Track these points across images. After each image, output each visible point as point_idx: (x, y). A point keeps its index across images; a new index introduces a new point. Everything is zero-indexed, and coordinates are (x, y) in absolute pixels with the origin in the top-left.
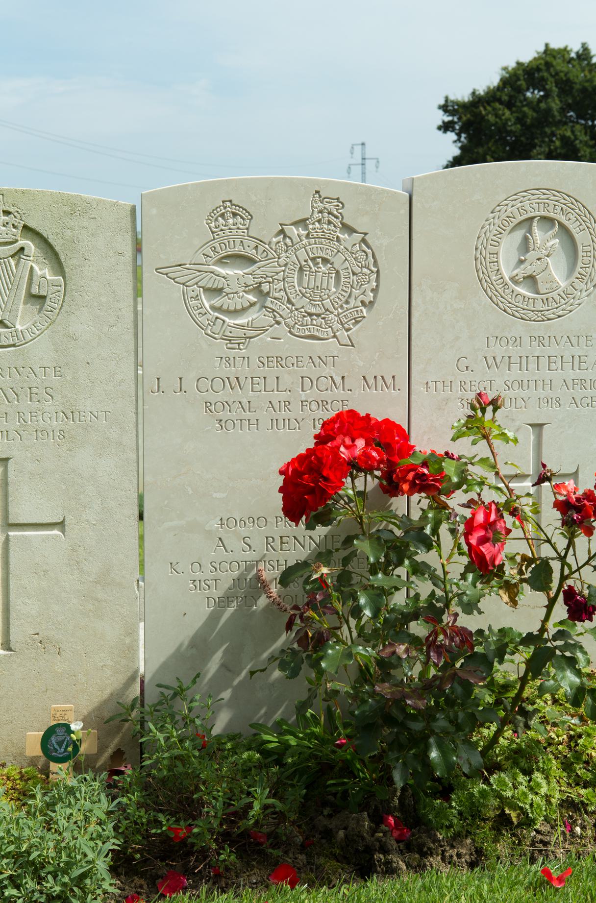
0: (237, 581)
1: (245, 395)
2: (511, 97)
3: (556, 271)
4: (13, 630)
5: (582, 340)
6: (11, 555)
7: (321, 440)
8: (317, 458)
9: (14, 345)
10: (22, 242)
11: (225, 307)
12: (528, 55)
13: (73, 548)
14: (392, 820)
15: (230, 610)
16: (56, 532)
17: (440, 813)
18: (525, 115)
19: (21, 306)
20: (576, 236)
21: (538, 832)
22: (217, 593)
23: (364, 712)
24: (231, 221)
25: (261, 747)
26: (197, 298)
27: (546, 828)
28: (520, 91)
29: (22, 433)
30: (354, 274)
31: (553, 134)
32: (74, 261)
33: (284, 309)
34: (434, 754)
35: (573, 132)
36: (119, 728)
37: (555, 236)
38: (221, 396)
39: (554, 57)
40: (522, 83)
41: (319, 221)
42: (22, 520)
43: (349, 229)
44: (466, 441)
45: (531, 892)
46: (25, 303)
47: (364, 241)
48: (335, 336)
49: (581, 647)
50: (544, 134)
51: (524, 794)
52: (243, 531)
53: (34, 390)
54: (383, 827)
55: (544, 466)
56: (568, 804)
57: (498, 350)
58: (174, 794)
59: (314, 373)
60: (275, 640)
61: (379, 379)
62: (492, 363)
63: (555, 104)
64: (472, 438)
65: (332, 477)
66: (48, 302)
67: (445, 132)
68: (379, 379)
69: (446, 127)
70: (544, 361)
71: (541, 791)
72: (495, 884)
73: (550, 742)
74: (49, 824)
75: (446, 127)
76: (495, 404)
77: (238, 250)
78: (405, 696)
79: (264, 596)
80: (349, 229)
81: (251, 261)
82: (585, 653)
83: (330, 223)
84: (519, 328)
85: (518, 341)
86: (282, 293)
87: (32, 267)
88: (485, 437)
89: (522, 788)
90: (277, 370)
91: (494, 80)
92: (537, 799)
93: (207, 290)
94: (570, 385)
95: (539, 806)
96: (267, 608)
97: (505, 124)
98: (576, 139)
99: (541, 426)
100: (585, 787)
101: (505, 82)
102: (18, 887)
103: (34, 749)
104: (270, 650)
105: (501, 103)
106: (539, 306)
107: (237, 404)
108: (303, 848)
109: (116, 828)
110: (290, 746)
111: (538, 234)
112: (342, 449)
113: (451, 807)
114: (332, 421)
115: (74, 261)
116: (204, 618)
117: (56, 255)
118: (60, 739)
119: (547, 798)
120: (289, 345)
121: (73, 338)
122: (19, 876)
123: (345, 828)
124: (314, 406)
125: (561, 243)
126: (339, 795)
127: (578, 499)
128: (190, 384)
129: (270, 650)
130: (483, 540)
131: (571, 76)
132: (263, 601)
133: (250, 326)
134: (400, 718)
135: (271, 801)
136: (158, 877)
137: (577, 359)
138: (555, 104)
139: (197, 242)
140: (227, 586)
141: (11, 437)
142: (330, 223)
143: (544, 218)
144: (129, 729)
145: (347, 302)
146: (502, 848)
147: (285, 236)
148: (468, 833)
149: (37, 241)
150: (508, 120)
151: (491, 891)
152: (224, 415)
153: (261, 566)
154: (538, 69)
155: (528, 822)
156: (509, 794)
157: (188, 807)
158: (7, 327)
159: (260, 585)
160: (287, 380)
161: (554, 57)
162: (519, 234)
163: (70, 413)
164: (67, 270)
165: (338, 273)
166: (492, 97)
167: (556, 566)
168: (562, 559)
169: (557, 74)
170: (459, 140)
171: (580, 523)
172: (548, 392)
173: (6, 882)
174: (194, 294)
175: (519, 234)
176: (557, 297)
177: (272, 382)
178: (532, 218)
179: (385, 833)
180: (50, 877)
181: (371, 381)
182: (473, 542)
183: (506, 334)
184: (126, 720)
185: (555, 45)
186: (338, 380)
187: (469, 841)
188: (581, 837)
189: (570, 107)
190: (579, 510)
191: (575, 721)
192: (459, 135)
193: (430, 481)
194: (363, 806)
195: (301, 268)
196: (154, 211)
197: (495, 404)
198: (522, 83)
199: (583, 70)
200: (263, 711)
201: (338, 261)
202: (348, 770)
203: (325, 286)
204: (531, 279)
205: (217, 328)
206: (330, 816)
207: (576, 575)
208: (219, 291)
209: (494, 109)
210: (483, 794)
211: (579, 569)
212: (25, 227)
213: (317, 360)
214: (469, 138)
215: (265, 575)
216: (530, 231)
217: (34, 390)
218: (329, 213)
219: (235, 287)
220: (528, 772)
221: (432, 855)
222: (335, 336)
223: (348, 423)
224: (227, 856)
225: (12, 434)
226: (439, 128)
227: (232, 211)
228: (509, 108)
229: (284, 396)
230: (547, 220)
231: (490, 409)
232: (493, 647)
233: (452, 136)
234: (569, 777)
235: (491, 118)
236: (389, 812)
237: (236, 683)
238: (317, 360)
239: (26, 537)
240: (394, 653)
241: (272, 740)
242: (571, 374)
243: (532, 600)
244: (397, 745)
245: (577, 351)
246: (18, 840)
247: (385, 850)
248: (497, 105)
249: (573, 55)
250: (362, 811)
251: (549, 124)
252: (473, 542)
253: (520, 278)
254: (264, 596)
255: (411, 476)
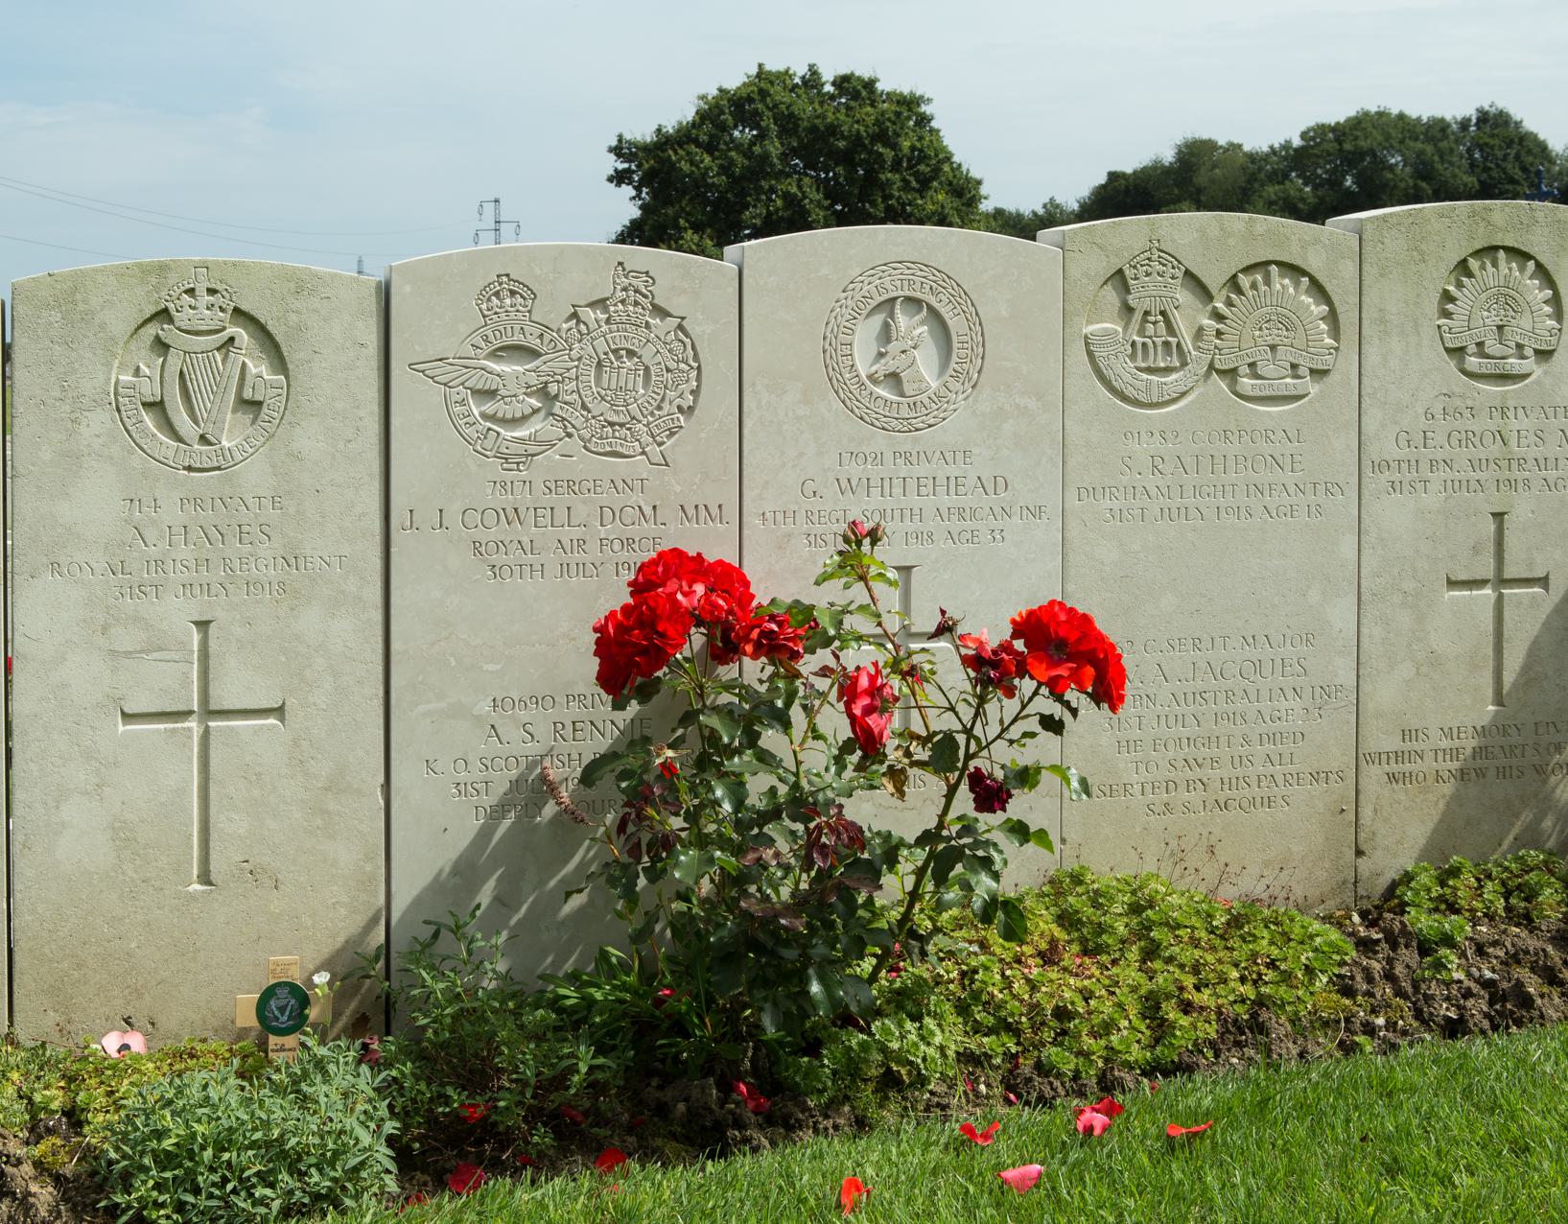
0: (516, 785)
1: (527, 532)
2: (711, 136)
3: (925, 365)
4: (214, 856)
5: (960, 456)
6: (212, 754)
7: (637, 588)
8: (649, 607)
9: (219, 468)
10: (231, 330)
11: (500, 415)
12: (735, 78)
13: (296, 742)
14: (743, 1088)
15: (507, 823)
16: (272, 721)
17: (810, 1073)
18: (732, 162)
19: (229, 416)
20: (950, 322)
21: (932, 1093)
22: (489, 801)
23: (721, 938)
24: (508, 301)
25: (555, 1004)
26: (463, 402)
27: (942, 1089)
28: (723, 128)
29: (228, 586)
30: (668, 370)
31: (772, 190)
32: (301, 355)
33: (577, 417)
34: (815, 988)
35: (800, 187)
36: (357, 988)
37: (922, 323)
38: (494, 533)
39: (772, 83)
40: (727, 117)
41: (623, 302)
42: (227, 705)
43: (661, 312)
44: (838, 583)
45: (953, 1154)
46: (234, 411)
47: (680, 327)
48: (644, 453)
49: (995, 845)
50: (759, 190)
51: (915, 1044)
52: (523, 715)
53: (246, 529)
54: (734, 1096)
55: (943, 612)
56: (967, 1057)
57: (855, 470)
58: (459, 1057)
59: (617, 500)
60: (566, 862)
61: (702, 508)
62: (846, 487)
63: (774, 148)
64: (844, 580)
65: (671, 632)
66: (265, 410)
67: (619, 185)
68: (702, 508)
69: (619, 178)
70: (912, 484)
71: (935, 1041)
72: (904, 1145)
73: (938, 981)
74: (304, 1101)
75: (619, 178)
76: (874, 536)
77: (518, 339)
78: (776, 916)
79: (552, 802)
80: (661, 312)
81: (534, 354)
82: (1001, 852)
83: (636, 303)
84: (880, 442)
85: (878, 458)
86: (575, 396)
87: (244, 364)
88: (863, 578)
89: (913, 1037)
90: (569, 498)
91: (689, 115)
92: (931, 1051)
93: (476, 392)
94: (945, 515)
95: (933, 1059)
96: (555, 820)
97: (705, 175)
98: (805, 197)
99: (909, 569)
100: (986, 1035)
101: (703, 116)
102: (272, 1186)
103: (248, 1019)
104: (559, 877)
105: (698, 145)
106: (905, 412)
107: (515, 544)
108: (630, 1130)
109: (391, 1107)
110: (596, 1001)
111: (902, 319)
112: (679, 596)
113: (823, 1066)
114: (653, 563)
115: (301, 355)
116: (471, 835)
117: (276, 347)
118: (283, 1002)
119: (942, 1049)
120: (584, 465)
121: (298, 457)
122: (271, 1171)
123: (686, 1100)
124: (617, 546)
125: (930, 332)
126: (669, 1061)
127: (994, 652)
128: (453, 518)
129: (559, 877)
130: (869, 710)
131: (794, 108)
132: (550, 810)
133: (533, 439)
134: (770, 944)
135: (601, 1061)
136: (446, 1171)
137: (953, 481)
138: (774, 148)
139: (464, 329)
140: (502, 790)
141: (213, 592)
142: (636, 303)
143: (908, 299)
144: (370, 989)
145: (659, 408)
146: (889, 1116)
147: (579, 321)
148: (847, 1098)
149: (251, 329)
150: (707, 169)
151: (902, 1154)
152: (498, 559)
153: (547, 763)
154: (750, 99)
155: (921, 1081)
156: (895, 1045)
157: (477, 1076)
158: (210, 444)
159: (546, 787)
160: (581, 512)
161: (772, 83)
162: (878, 319)
163: (292, 559)
164: (290, 367)
165: (647, 369)
166: (684, 137)
167: (961, 739)
168: (968, 732)
169: (776, 106)
170: (638, 196)
171: (997, 683)
172: (916, 525)
173: (254, 1180)
174: (459, 398)
175: (878, 319)
176: (926, 401)
177: (561, 515)
178: (895, 299)
179: (737, 1104)
180: (313, 1170)
181: (691, 512)
182: (857, 712)
183: (864, 449)
184: (369, 977)
185: (773, 66)
186: (648, 510)
187: (847, 1109)
188: (988, 1097)
189: (795, 152)
190: (995, 664)
191: (975, 948)
192: (638, 189)
193: (783, 637)
194: (707, 1071)
195: (599, 363)
196: (408, 288)
197: (874, 536)
198: (727, 117)
199: (812, 103)
200: (549, 960)
201: (647, 353)
202: (680, 1027)
203: (630, 386)
204: (894, 378)
205: (488, 444)
206: (661, 1087)
207: (985, 753)
208: (491, 394)
209: (688, 154)
210: (863, 1045)
211: (988, 745)
212: (237, 310)
213: (620, 485)
214: (654, 194)
215: (553, 774)
216: (892, 315)
217: (246, 529)
218: (636, 291)
219: (513, 388)
220: (916, 1018)
221: (801, 1128)
222: (644, 453)
223: (675, 564)
224: (541, 1138)
225: (216, 588)
226: (610, 179)
227: (509, 288)
228: (711, 153)
229: (577, 532)
230: (914, 303)
231: (867, 541)
232: (878, 851)
233: (628, 191)
234: (965, 1024)
235: (685, 166)
236: (740, 1078)
237: (513, 922)
238: (620, 485)
239: (232, 729)
240: (760, 858)
241: (570, 995)
242: (946, 501)
243: (925, 789)
244: (760, 982)
245: (953, 471)
246: (266, 1125)
247: (740, 1126)
248: (693, 148)
249: (797, 80)
250: (705, 1077)
251: (767, 176)
252: (857, 712)
253: (880, 375)
254: (552, 802)
255: (755, 634)
